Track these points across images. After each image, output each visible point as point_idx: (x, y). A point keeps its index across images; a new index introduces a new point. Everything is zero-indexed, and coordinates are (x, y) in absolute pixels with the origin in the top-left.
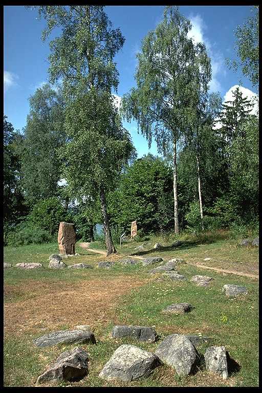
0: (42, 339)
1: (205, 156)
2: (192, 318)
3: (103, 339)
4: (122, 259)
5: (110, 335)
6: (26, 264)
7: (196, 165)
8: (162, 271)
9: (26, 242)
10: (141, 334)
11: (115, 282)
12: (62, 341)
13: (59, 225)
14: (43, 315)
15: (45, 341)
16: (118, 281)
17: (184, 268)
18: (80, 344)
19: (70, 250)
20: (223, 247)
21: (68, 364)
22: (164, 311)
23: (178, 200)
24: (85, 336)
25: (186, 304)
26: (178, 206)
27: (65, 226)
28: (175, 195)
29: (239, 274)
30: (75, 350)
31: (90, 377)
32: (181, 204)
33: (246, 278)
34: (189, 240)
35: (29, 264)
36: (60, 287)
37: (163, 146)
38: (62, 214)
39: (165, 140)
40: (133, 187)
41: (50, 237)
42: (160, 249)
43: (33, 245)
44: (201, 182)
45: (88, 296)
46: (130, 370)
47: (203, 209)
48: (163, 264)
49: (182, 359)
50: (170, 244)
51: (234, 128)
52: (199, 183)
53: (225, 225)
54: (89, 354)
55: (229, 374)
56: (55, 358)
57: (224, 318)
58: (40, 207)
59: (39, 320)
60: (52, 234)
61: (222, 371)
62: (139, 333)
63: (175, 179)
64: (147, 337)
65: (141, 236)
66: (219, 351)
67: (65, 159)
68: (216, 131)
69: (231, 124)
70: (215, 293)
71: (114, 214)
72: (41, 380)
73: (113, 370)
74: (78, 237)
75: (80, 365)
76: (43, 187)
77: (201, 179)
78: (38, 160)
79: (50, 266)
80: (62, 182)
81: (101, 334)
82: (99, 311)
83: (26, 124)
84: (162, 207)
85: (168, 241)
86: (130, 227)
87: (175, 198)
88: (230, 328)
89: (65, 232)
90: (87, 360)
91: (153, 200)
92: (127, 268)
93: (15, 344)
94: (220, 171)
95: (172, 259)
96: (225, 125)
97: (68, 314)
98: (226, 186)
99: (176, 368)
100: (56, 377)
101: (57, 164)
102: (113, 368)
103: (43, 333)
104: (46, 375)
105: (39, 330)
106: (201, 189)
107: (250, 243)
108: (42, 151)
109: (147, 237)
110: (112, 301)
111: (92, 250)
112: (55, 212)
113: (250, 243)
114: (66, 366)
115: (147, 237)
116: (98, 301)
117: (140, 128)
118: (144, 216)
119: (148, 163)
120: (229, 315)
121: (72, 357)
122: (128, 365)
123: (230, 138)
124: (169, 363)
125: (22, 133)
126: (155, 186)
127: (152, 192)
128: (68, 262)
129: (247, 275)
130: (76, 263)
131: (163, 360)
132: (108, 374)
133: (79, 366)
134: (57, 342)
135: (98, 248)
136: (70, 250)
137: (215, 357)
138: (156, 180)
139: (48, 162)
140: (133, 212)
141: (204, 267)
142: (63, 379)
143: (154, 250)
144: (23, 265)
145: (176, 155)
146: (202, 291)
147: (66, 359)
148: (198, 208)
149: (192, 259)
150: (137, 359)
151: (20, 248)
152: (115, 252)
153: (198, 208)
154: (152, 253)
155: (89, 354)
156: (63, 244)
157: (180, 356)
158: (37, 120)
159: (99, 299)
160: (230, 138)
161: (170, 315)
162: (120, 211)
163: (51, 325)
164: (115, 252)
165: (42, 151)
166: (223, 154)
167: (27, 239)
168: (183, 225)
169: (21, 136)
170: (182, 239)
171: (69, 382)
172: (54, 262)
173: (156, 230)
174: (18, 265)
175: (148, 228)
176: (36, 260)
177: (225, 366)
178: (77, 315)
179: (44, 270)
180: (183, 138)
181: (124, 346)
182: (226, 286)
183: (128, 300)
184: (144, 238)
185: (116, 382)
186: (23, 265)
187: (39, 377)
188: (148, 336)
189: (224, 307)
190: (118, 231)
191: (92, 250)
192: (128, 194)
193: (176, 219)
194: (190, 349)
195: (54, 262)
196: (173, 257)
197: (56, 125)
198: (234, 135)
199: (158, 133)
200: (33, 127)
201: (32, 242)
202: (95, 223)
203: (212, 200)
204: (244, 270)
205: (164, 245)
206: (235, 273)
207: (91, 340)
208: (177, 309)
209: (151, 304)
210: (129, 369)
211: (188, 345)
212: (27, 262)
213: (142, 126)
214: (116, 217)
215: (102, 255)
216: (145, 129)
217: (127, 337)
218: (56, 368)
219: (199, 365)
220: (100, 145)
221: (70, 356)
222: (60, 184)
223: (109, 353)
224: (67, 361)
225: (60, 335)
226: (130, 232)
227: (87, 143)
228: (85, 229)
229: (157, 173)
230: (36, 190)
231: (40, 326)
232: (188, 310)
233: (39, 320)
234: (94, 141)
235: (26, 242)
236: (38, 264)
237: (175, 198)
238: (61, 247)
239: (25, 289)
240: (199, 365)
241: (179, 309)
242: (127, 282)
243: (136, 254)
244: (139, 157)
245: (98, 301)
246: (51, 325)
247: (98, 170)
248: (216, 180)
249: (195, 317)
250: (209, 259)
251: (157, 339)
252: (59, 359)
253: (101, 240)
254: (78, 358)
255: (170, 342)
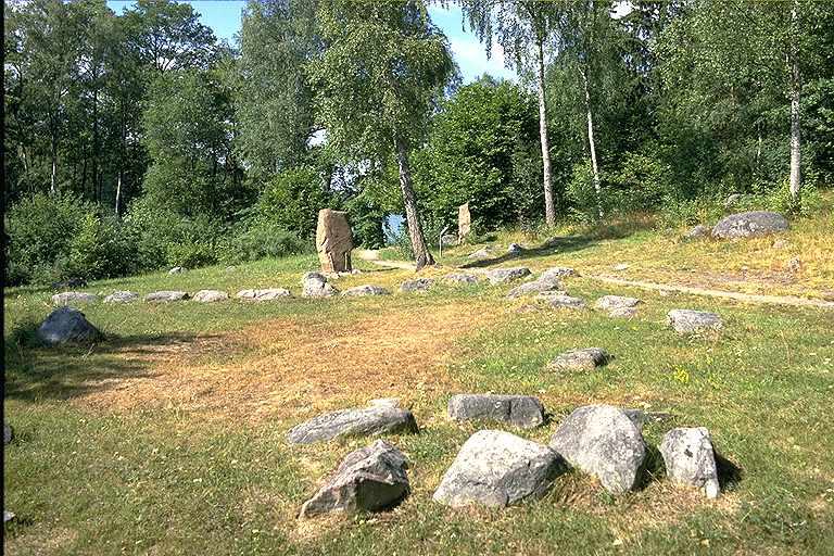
0: (303, 427)
1: (600, 70)
2: (612, 378)
3: (431, 423)
4: (446, 273)
5: (446, 414)
6: (257, 291)
7: (580, 87)
8: (533, 292)
9: (253, 254)
10: (513, 411)
11: (439, 316)
12: (347, 430)
13: (316, 219)
14: (300, 383)
15: (310, 432)
16: (446, 314)
17: (577, 285)
18: (386, 434)
19: (342, 264)
20: (654, 242)
21: (365, 475)
22: (549, 365)
23: (550, 159)
24: (395, 419)
25: (597, 350)
26: (551, 170)
27: (329, 218)
28: (544, 148)
29: (696, 291)
30: (376, 448)
31: (414, 501)
32: (556, 166)
33: (710, 298)
34: (577, 235)
35: (263, 292)
36: (330, 330)
37: (516, 52)
38: (320, 197)
39: (518, 41)
40: (458, 138)
41: (299, 242)
42: (520, 252)
43: (267, 260)
44: (594, 123)
45: (389, 342)
46: (500, 484)
47: (600, 177)
48: (532, 280)
49: (615, 457)
50: (537, 245)
51: (656, 12)
52: (590, 124)
53: (652, 203)
54: (408, 455)
55: (721, 486)
56: (337, 465)
57: (681, 375)
58: (276, 189)
59: (292, 392)
60: (304, 236)
61: (704, 480)
62: (508, 409)
63: (542, 117)
64: (525, 416)
65: (479, 233)
66: (694, 437)
67: (320, 85)
68: (618, 22)
69: (649, 5)
70: (652, 328)
71: (423, 194)
72: (309, 510)
73: (465, 484)
74: (356, 242)
75: (390, 476)
76: (281, 149)
77: (593, 116)
78: (269, 96)
79: (304, 294)
80: (318, 139)
81: (425, 414)
82: (415, 370)
83: (239, 27)
84: (520, 172)
85: (534, 238)
86: (456, 217)
87: (545, 155)
88: (699, 395)
89: (329, 228)
90: (405, 466)
91: (502, 161)
92: (460, 291)
93: (249, 441)
94: (631, 100)
95: (549, 269)
96: (638, 8)
97: (351, 378)
98: (648, 123)
99: (601, 477)
100: (342, 504)
101: (307, 94)
102: (464, 481)
103: (303, 418)
104: (320, 500)
105: (295, 412)
106: (594, 137)
107: (707, 234)
108: (273, 79)
109: (492, 234)
110: (439, 350)
111: (383, 263)
112: (305, 196)
113: (707, 234)
114: (362, 480)
115: (492, 234)
116: (409, 352)
117: (467, 20)
118: (484, 195)
119: (485, 91)
120: (692, 370)
121: (373, 460)
122: (497, 473)
123: (648, 34)
124: (584, 467)
125: (235, 46)
126: (503, 133)
127: (497, 144)
128: (339, 286)
129: (708, 292)
130: (356, 286)
131: (571, 460)
132: (454, 493)
133: (389, 479)
134: (336, 432)
135: (395, 258)
136: (342, 264)
137: (687, 453)
138: (504, 120)
139: (288, 97)
140: (460, 187)
141: (615, 280)
142: (358, 507)
143: (507, 257)
144: (250, 293)
145: (542, 69)
146: (624, 326)
147: (360, 465)
148: (588, 171)
149: (590, 268)
150: (516, 460)
151: (243, 266)
152: (432, 262)
153: (588, 171)
154: (506, 263)
155: (408, 455)
156: (327, 252)
157: (609, 449)
158: (260, 17)
159: (412, 347)
160: (648, 34)
161: (566, 374)
162: (434, 186)
163: (318, 401)
164: (432, 262)
165: (273, 79)
166: (635, 66)
167: (254, 248)
168: (563, 208)
169: (233, 52)
170: (563, 232)
171: (370, 514)
172: (311, 286)
173: (510, 221)
174: (240, 295)
175: (493, 216)
176: (275, 284)
177: (711, 469)
178: (370, 380)
179: (293, 299)
180: (554, 36)
181: (484, 433)
182: (674, 313)
183: (473, 348)
184: (483, 238)
185: (473, 509)
186: (250, 293)
187: (306, 503)
188: (529, 415)
189: (676, 355)
190: (433, 225)
191: (383, 263)
192: (451, 153)
193: (548, 196)
194: (631, 434)
195: (311, 286)
196: (548, 266)
197: (300, 25)
198: (657, 25)
199: (505, 26)
200: (254, 31)
201: (265, 254)
202: (387, 214)
203: (617, 157)
204: (702, 283)
205: (527, 245)
206: (684, 290)
207: (408, 425)
208: (578, 358)
209: (522, 352)
210: (500, 481)
211: (627, 427)
212: (258, 287)
213: (473, 15)
214: (427, 197)
215: (406, 270)
216: (478, 20)
217: (484, 416)
218: (340, 483)
219: (653, 469)
220: (392, 49)
221: (368, 460)
222: (314, 141)
223: (452, 451)
224: (363, 469)
225: (341, 419)
226: (457, 227)
227: (361, 55)
228: (367, 225)
229: (506, 109)
230: (267, 157)
231: (296, 404)
232: (601, 361)
233: (292, 392)
234: (379, 43)
235: (253, 254)
236: (281, 291)
237: (545, 155)
238: (324, 258)
239: (260, 337)
240: (653, 469)
241: (582, 360)
242: (463, 315)
243: (474, 265)
244: (466, 83)
245: (409, 352)
246: (318, 401)
247: (390, 101)
248: (624, 120)
249: (617, 374)
250: (625, 265)
251: (547, 419)
252: (343, 468)
253: (400, 242)
254: (386, 463)
255: (583, 421)
